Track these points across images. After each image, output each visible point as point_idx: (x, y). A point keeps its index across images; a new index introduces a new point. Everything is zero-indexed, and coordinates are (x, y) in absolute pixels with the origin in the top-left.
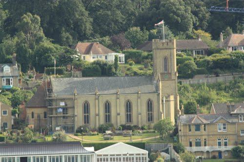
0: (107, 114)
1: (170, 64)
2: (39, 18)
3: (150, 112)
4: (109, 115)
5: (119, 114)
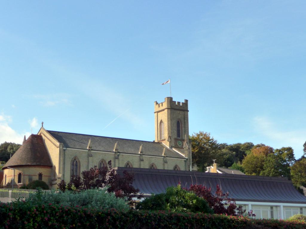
1: (183, 129)
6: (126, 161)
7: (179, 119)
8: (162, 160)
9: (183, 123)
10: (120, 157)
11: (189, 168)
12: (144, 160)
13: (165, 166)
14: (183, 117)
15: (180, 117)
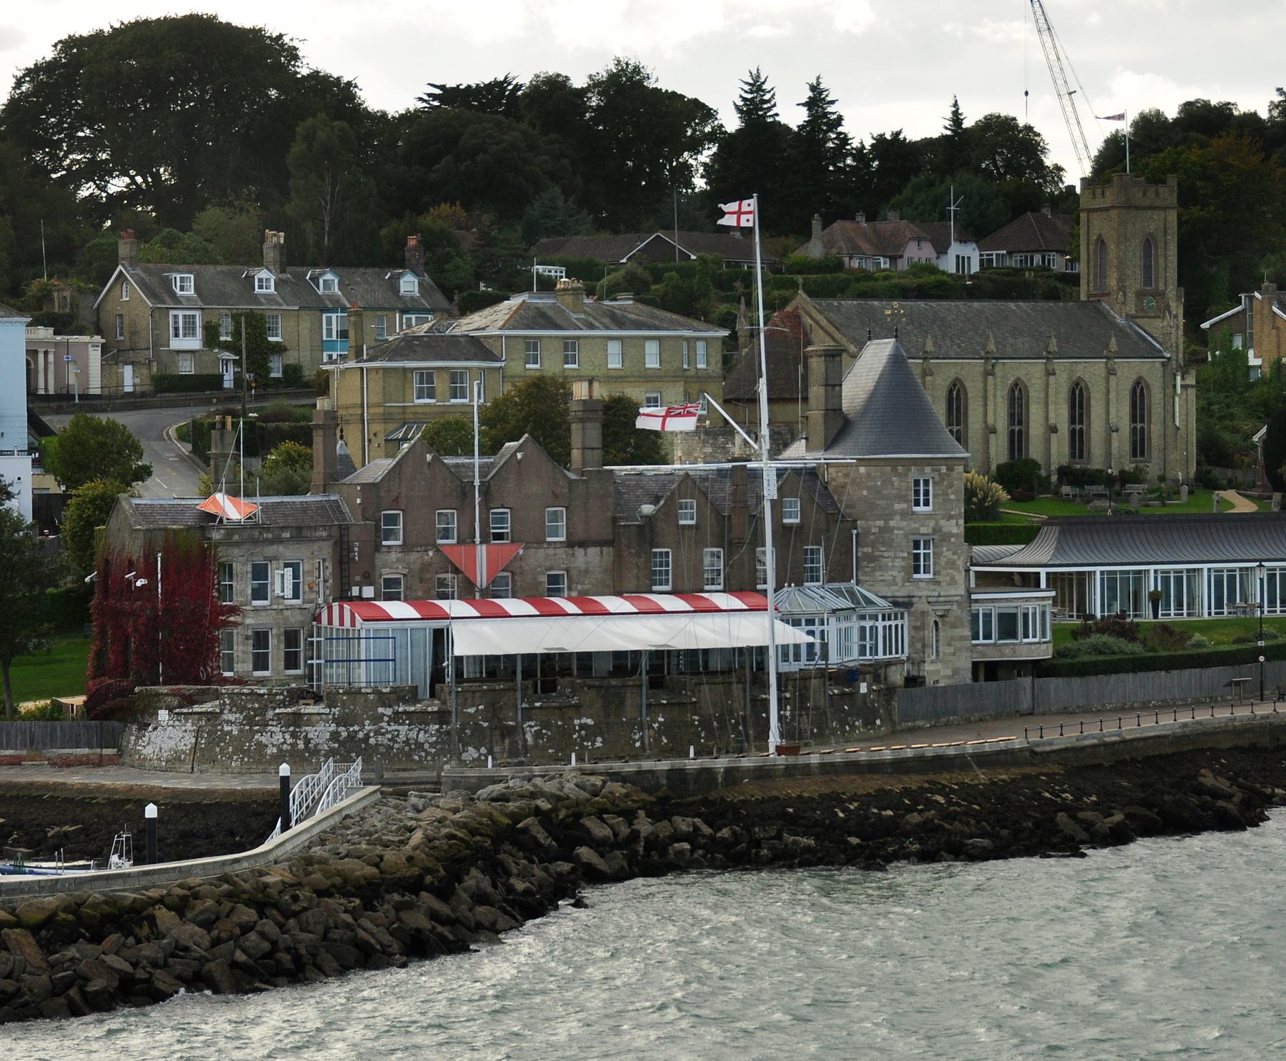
0: (1017, 428)
1: (1161, 260)
2: (384, 690)
3: (1139, 426)
4: (1020, 431)
5: (1054, 430)
6: (1013, 379)
7: (1150, 234)
8: (1103, 366)
9: (1161, 245)
10: (997, 369)
11: (1175, 379)
12: (1057, 372)
13: (1111, 383)
14: (1161, 225)
15: (1152, 228)
